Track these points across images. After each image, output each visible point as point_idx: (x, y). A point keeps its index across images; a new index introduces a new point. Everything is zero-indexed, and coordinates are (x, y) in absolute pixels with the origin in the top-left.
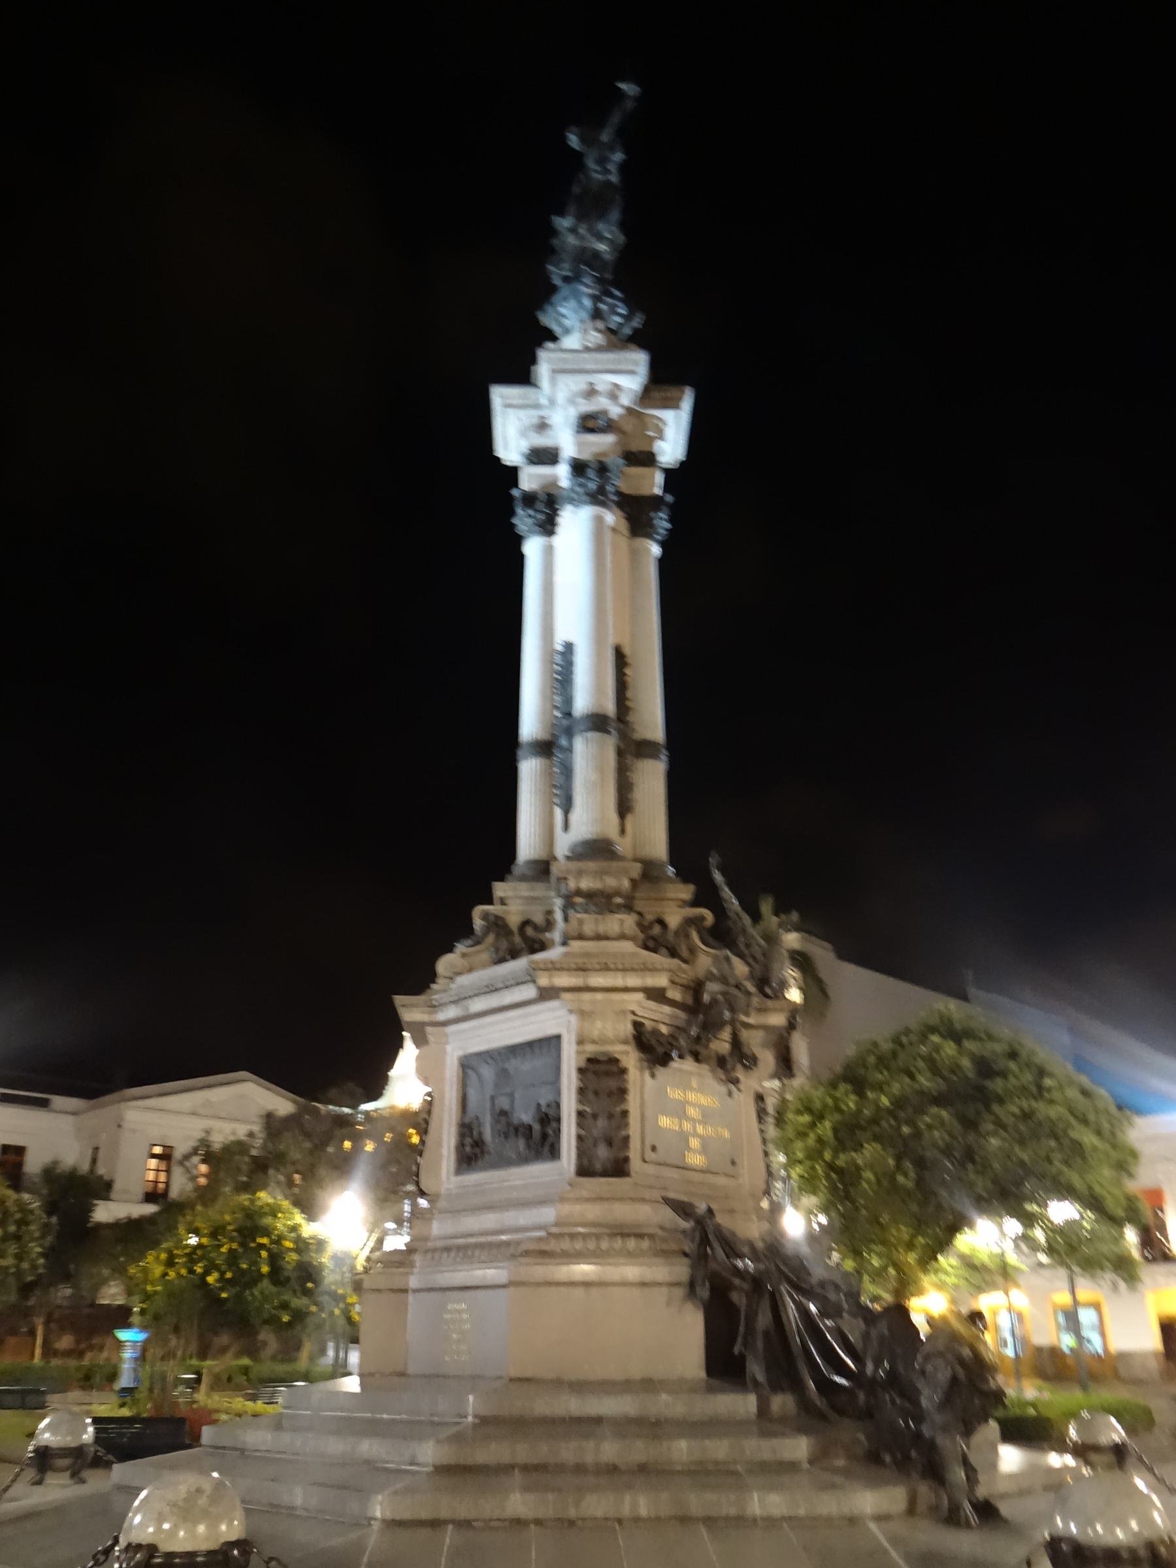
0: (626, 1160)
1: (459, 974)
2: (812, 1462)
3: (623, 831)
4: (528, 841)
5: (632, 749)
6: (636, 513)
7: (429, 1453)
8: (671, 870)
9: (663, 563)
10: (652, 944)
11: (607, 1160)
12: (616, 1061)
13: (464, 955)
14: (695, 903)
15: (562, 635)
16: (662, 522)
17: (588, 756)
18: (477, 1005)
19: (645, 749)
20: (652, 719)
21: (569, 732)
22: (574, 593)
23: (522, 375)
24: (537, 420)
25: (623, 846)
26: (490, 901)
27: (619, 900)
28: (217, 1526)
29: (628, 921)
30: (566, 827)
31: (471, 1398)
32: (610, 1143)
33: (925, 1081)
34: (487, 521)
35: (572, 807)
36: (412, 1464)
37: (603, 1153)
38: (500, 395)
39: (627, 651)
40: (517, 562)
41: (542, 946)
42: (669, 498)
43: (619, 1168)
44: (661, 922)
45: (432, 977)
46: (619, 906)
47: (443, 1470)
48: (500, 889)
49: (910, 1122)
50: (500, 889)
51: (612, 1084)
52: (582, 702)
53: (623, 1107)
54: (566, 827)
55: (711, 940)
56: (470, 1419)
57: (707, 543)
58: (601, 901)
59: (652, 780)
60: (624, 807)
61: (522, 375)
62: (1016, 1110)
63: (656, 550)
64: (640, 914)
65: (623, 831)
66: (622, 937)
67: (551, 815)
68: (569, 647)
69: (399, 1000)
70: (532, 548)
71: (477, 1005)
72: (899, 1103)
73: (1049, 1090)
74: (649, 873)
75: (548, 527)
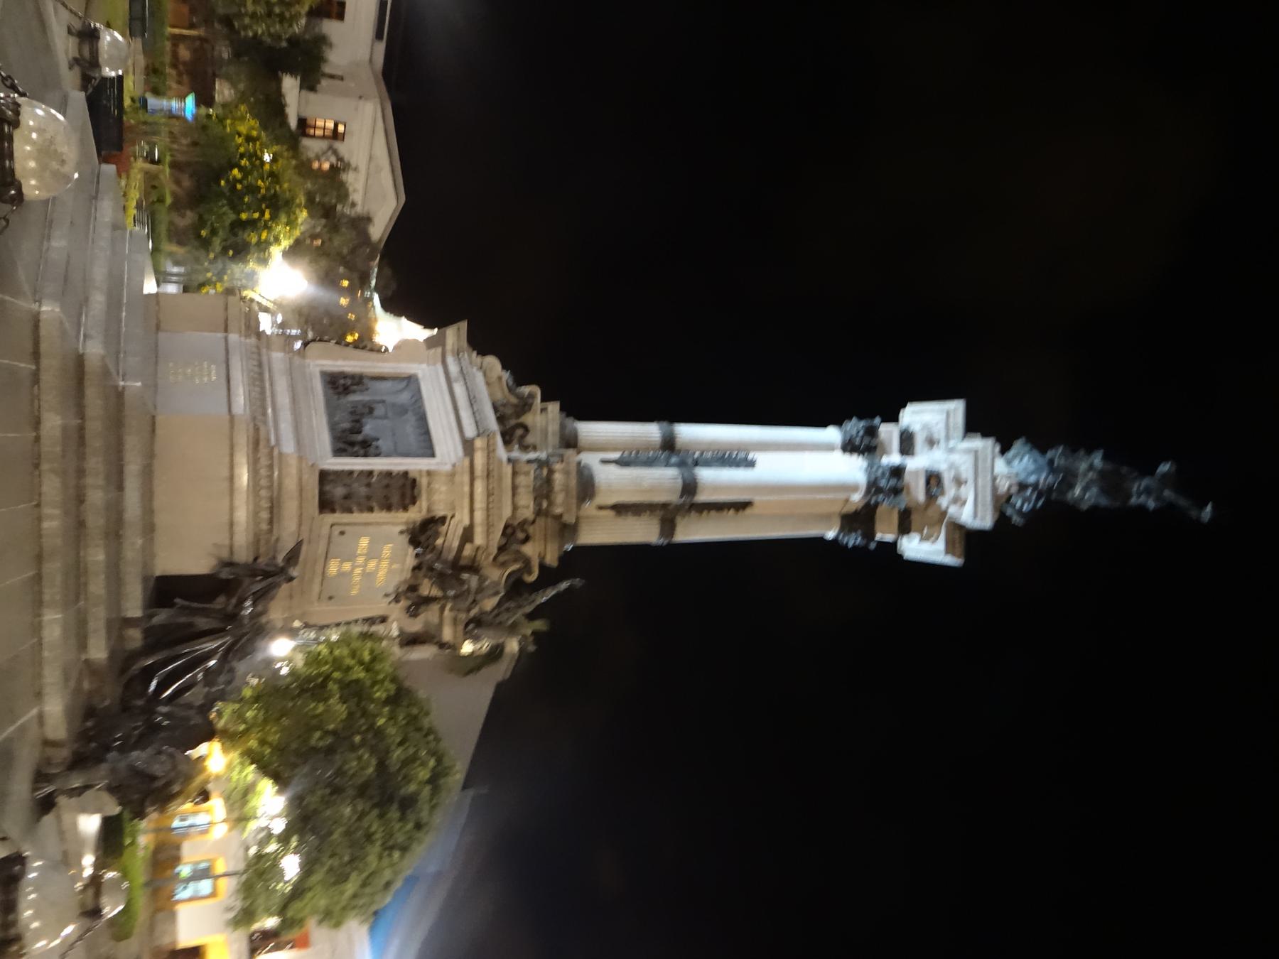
0: (333, 511)
1: (485, 375)
2: (87, 661)
3: (601, 508)
4: (591, 430)
5: (668, 515)
6: (861, 519)
7: (94, 350)
8: (569, 547)
9: (820, 540)
10: (510, 532)
11: (333, 495)
12: (414, 503)
13: (500, 378)
14: (542, 567)
15: (760, 458)
16: (853, 540)
17: (661, 480)
18: (459, 389)
19: (668, 526)
20: (692, 532)
21: (681, 464)
22: (794, 469)
23: (973, 426)
24: (934, 436)
25: (589, 508)
26: (544, 399)
27: (545, 504)
28: (33, 177)
29: (527, 512)
30: (605, 462)
31: (139, 384)
32: (347, 497)
33: (397, 754)
34: (853, 395)
35: (621, 467)
36: (85, 336)
37: (339, 491)
38: (956, 409)
39: (748, 511)
40: (822, 423)
41: (507, 442)
42: (873, 546)
43: (326, 505)
44: (526, 539)
45: (482, 352)
46: (540, 505)
47: (80, 361)
48: (554, 407)
49: (363, 741)
50: (554, 407)
51: (395, 499)
52: (706, 475)
53: (376, 508)
54: (605, 462)
55: (512, 579)
56: (122, 383)
57: (840, 572)
58: (544, 490)
59: (644, 532)
60: (621, 509)
61: (973, 426)
62: (373, 829)
63: (830, 535)
64: (534, 522)
65: (601, 508)
66: (515, 508)
67: (615, 449)
68: (751, 464)
69: (463, 325)
70: (832, 434)
71: (459, 389)
72: (379, 733)
73: (390, 855)
74: (567, 530)
75: (850, 447)
